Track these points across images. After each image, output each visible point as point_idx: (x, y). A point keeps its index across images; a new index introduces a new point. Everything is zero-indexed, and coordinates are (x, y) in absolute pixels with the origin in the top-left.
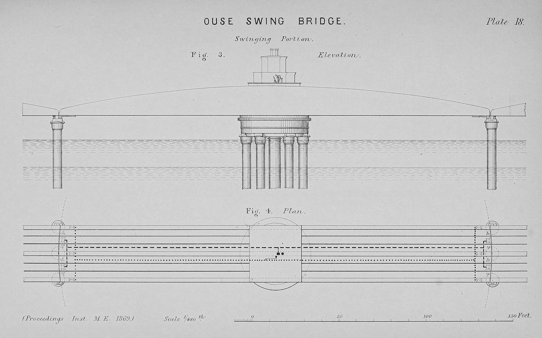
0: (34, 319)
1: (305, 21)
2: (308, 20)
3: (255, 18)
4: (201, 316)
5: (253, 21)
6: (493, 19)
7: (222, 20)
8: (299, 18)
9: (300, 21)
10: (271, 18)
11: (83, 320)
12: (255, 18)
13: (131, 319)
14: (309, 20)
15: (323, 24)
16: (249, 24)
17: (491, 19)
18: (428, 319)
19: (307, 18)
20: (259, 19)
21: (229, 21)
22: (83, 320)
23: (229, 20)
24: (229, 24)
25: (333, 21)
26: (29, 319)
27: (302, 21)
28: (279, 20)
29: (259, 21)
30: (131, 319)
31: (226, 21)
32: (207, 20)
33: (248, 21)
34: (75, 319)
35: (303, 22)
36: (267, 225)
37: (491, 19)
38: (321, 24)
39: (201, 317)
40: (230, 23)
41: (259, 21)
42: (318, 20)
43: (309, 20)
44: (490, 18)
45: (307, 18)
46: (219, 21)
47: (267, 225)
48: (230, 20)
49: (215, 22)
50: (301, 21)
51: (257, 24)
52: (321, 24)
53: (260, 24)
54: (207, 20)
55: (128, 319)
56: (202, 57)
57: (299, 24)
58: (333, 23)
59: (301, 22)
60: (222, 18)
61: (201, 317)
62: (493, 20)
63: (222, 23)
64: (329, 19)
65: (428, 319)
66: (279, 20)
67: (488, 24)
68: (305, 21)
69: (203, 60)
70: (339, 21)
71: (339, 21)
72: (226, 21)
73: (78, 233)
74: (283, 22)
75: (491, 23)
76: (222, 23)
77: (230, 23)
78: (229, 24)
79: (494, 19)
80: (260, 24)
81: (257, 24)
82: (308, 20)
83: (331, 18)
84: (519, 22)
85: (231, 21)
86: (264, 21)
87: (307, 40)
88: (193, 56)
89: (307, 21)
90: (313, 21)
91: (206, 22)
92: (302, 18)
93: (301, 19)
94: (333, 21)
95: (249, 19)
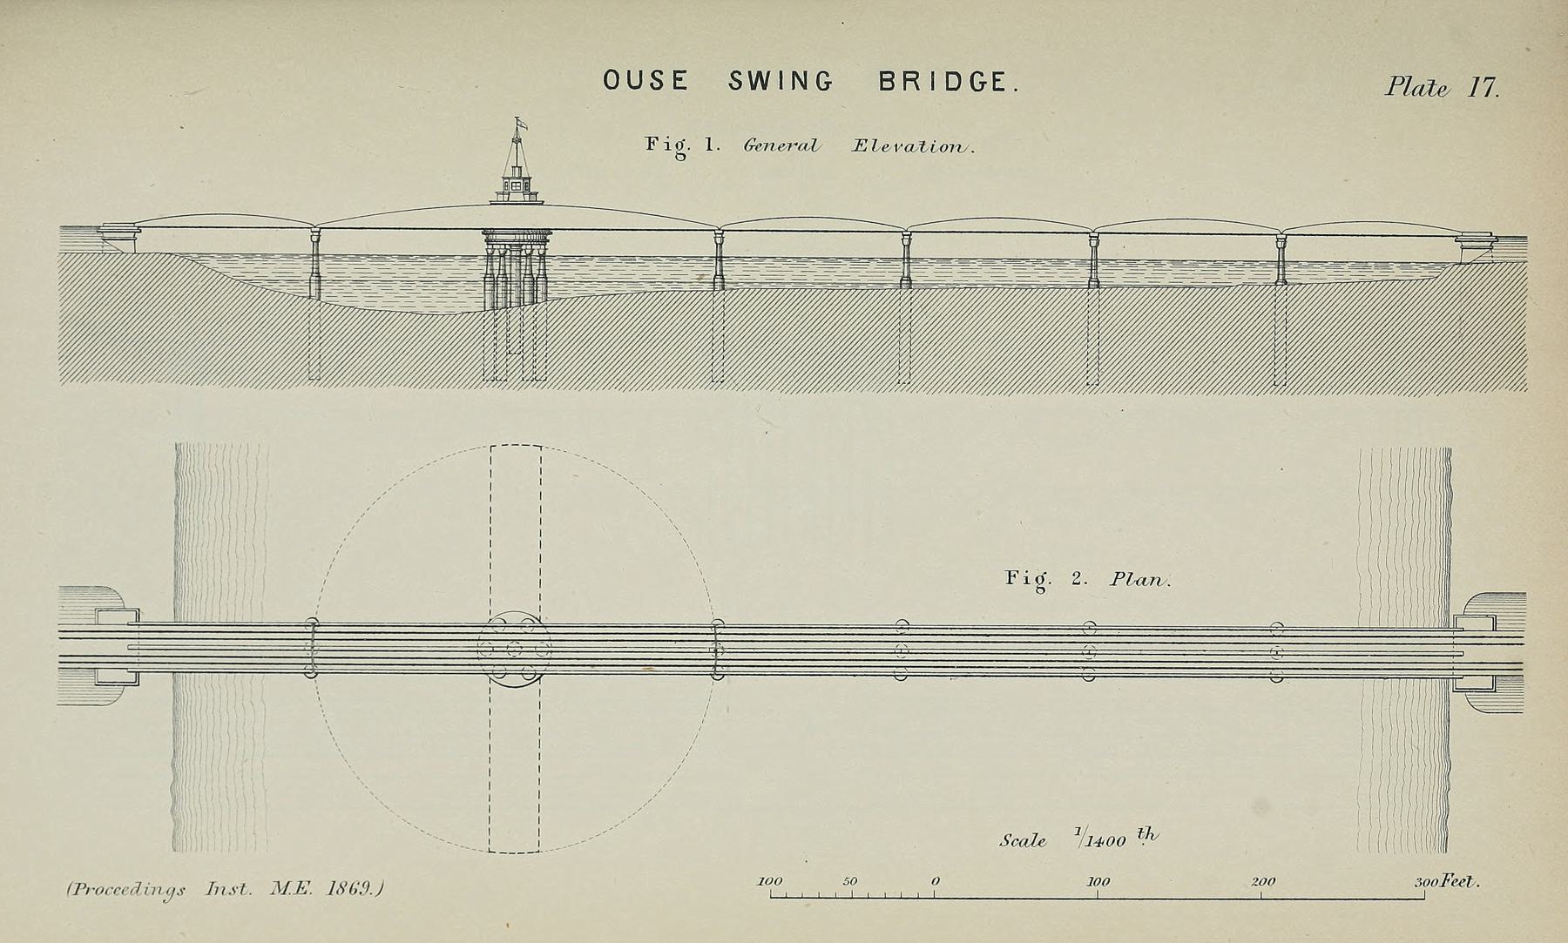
0: (99, 892)
1: (898, 80)
2: (885, 76)
3: (750, 72)
5: (744, 79)
6: (1407, 79)
8: (882, 73)
9: (882, 80)
11: (177, 890)
12: (750, 72)
13: (374, 889)
14: (911, 77)
15: (956, 89)
16: (736, 89)
17: (1399, 81)
18: (1267, 891)
19: (905, 73)
20: (759, 74)
21: (676, 79)
22: (177, 890)
23: (881, 76)
24: (675, 87)
25: (983, 83)
26: (82, 892)
27: (891, 80)
29: (760, 80)
30: (374, 889)
31: (667, 79)
34: (214, 889)
37: (1399, 81)
38: (948, 89)
39: (1146, 833)
40: (677, 86)
41: (760, 80)
43: (911, 77)
45: (905, 73)
46: (647, 79)
48: (997, 76)
49: (635, 82)
50: (886, 79)
51: (754, 87)
52: (948, 89)
53: (764, 87)
55: (364, 891)
57: (882, 89)
58: (982, 88)
59: (887, 85)
61: (1146, 833)
63: (657, 84)
65: (1267, 891)
67: (1390, 94)
68: (898, 80)
72: (667, 79)
73: (718, 631)
74: (828, 83)
75: (1399, 90)
76: (654, 85)
77: (677, 86)
79: (1410, 79)
80: (764, 87)
81: (754, 87)
84: (1483, 85)
85: (999, 80)
86: (773, 81)
88: (668, 149)
89: (906, 80)
90: (924, 81)
91: (611, 79)
95: (657, 75)
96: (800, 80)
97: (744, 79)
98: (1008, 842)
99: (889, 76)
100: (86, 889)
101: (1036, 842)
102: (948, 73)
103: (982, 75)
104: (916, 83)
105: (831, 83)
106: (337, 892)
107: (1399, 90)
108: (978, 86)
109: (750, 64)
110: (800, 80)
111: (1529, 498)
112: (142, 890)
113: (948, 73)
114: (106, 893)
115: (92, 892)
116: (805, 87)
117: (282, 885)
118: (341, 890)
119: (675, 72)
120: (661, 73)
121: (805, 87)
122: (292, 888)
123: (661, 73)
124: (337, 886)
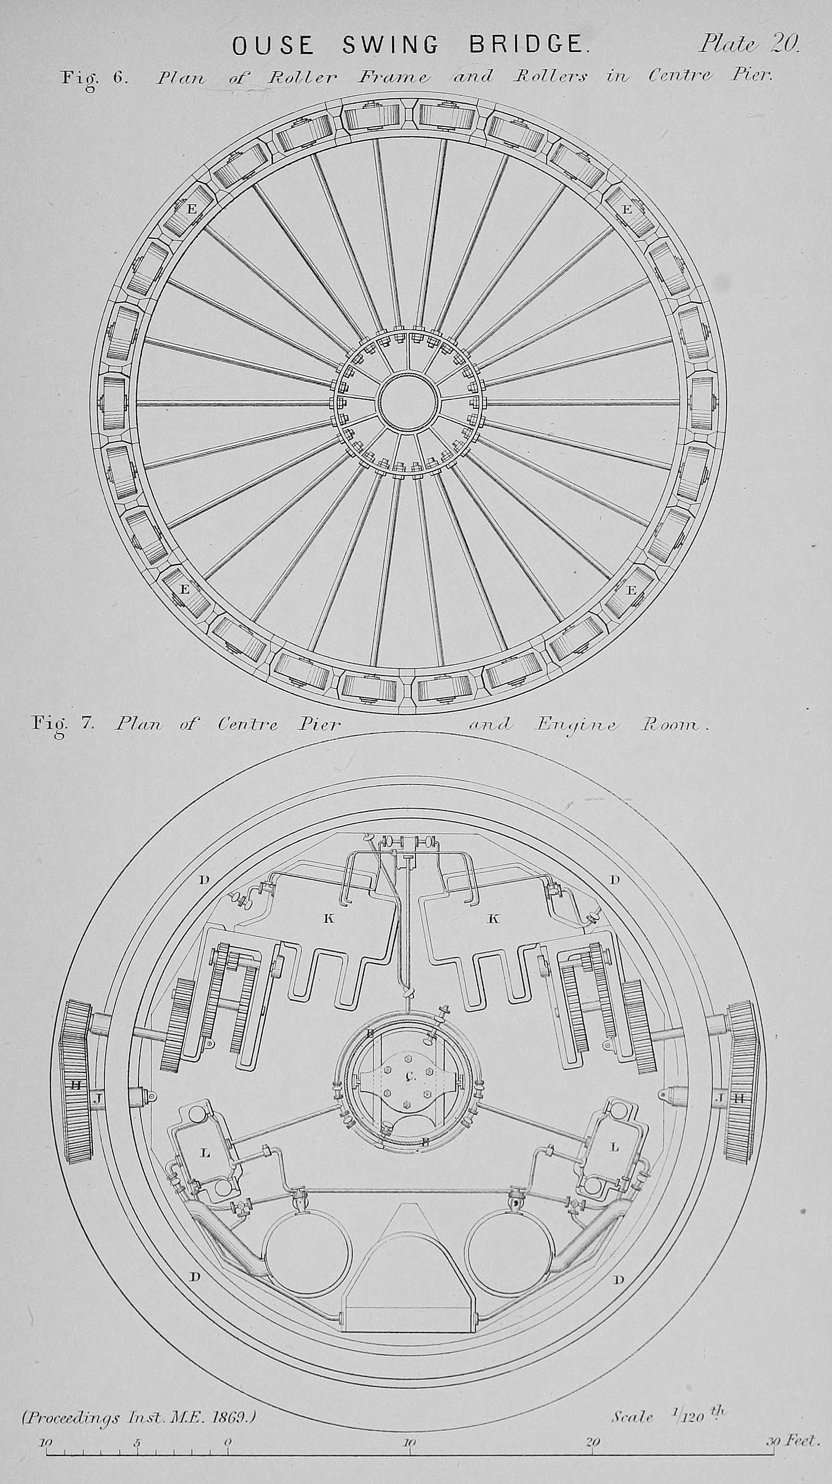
1: (488, 43)
2: (497, 39)
4: (717, 1408)
5: (358, 44)
7: (285, 42)
9: (472, 44)
10: (405, 37)
11: (113, 1419)
13: (248, 1417)
14: (498, 40)
17: (712, 38)
20: (372, 38)
22: (113, 1419)
25: (559, 46)
26: (35, 1420)
27: (480, 43)
28: (426, 40)
30: (248, 1417)
32: (240, 43)
33: (284, 47)
35: (482, 46)
36: (201, 933)
37: (712, 38)
39: (718, 1410)
42: (522, 43)
43: (498, 40)
44: (709, 35)
46: (277, 44)
47: (201, 933)
48: (573, 39)
49: (263, 48)
51: (367, 51)
54: (240, 43)
55: (239, 1420)
56: (85, 84)
58: (559, 49)
59: (477, 47)
60: (345, 39)
61: (718, 1410)
62: (717, 40)
64: (269, 49)
66: (426, 40)
68: (488, 43)
69: (86, 89)
70: (576, 43)
71: (576, 43)
72: (296, 44)
74: (434, 47)
75: (711, 46)
78: (472, 51)
80: (377, 51)
81: (367, 51)
82: (497, 39)
83: (429, 36)
86: (386, 45)
87: (675, 76)
90: (510, 44)
92: (479, 36)
93: (475, 40)
94: (559, 46)
96: (375, 47)
97: (358, 44)
98: (618, 1418)
99: (479, 40)
100: (39, 1417)
101: (644, 1419)
102: (528, 36)
103: (435, 39)
104: (503, 46)
105: (561, 45)
106: (220, 1421)
107: (711, 46)
108: (430, 49)
109: (360, 31)
110: (375, 47)
111: (313, 1080)
112: (84, 1419)
113: (528, 36)
114: (671, 728)
115: (44, 1420)
116: (415, 51)
117: (180, 1414)
118: (223, 1419)
119: (302, 37)
120: (291, 39)
121: (415, 51)
122: (188, 1417)
123: (291, 39)
124: (219, 1416)
